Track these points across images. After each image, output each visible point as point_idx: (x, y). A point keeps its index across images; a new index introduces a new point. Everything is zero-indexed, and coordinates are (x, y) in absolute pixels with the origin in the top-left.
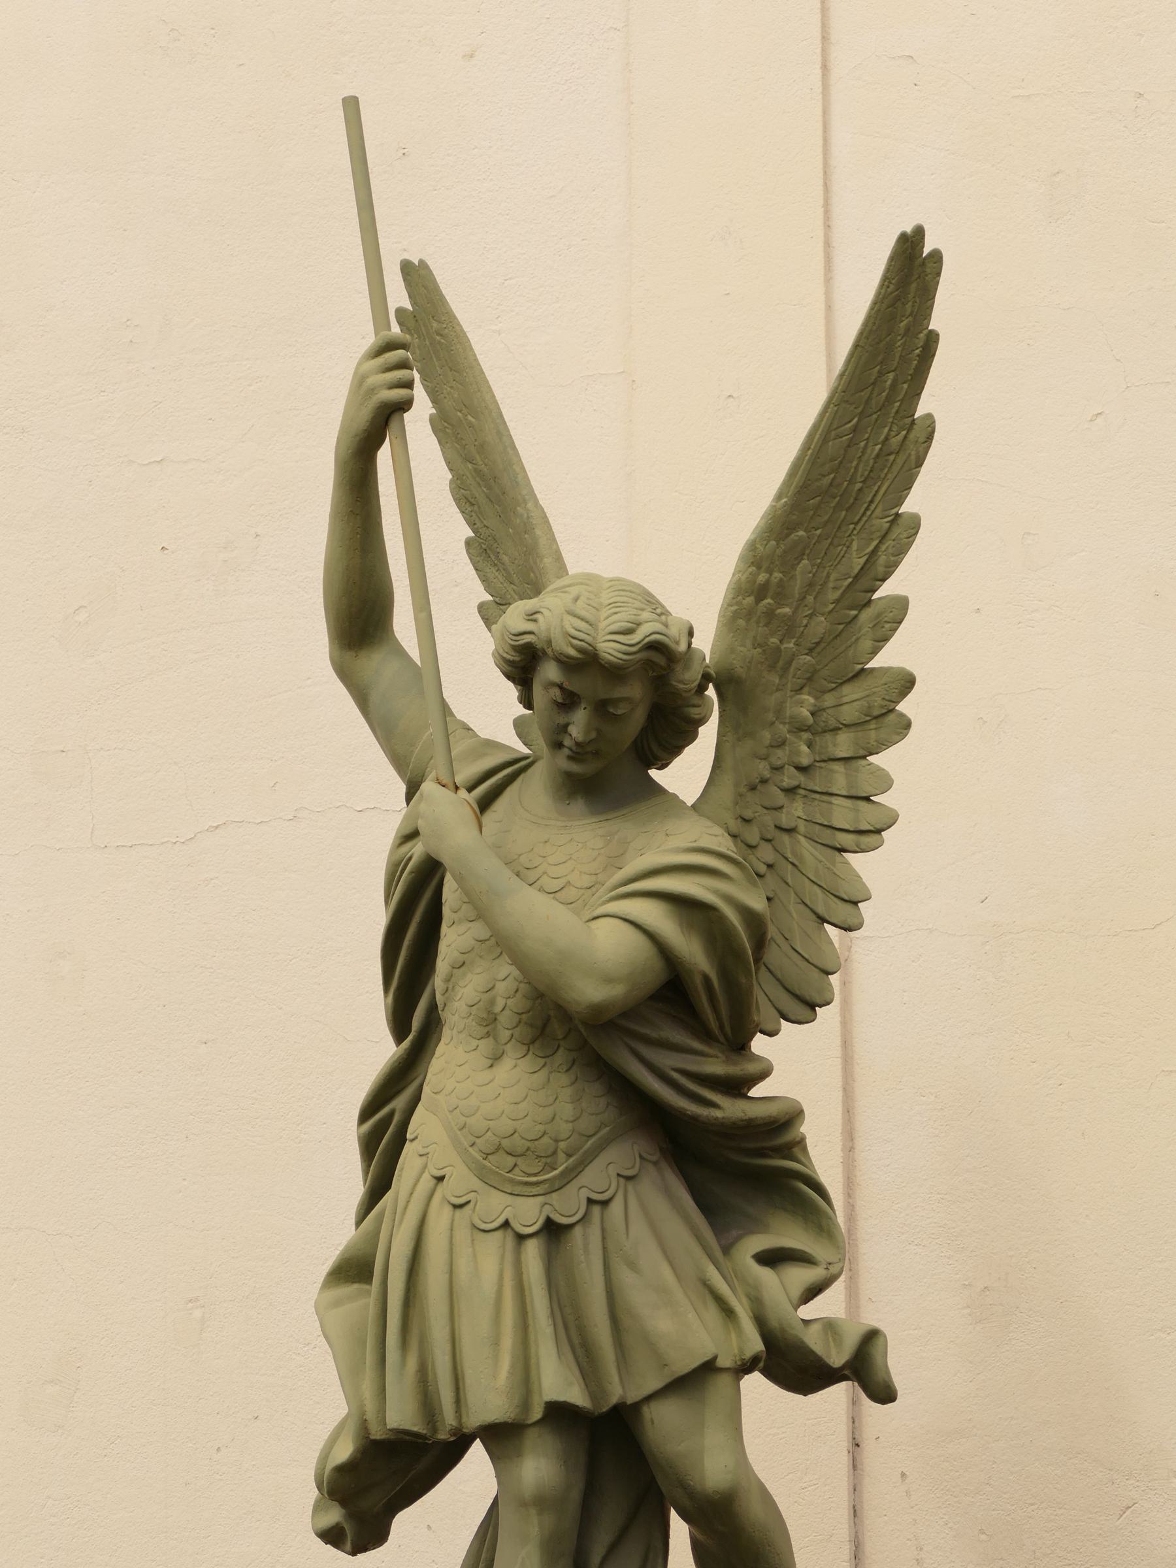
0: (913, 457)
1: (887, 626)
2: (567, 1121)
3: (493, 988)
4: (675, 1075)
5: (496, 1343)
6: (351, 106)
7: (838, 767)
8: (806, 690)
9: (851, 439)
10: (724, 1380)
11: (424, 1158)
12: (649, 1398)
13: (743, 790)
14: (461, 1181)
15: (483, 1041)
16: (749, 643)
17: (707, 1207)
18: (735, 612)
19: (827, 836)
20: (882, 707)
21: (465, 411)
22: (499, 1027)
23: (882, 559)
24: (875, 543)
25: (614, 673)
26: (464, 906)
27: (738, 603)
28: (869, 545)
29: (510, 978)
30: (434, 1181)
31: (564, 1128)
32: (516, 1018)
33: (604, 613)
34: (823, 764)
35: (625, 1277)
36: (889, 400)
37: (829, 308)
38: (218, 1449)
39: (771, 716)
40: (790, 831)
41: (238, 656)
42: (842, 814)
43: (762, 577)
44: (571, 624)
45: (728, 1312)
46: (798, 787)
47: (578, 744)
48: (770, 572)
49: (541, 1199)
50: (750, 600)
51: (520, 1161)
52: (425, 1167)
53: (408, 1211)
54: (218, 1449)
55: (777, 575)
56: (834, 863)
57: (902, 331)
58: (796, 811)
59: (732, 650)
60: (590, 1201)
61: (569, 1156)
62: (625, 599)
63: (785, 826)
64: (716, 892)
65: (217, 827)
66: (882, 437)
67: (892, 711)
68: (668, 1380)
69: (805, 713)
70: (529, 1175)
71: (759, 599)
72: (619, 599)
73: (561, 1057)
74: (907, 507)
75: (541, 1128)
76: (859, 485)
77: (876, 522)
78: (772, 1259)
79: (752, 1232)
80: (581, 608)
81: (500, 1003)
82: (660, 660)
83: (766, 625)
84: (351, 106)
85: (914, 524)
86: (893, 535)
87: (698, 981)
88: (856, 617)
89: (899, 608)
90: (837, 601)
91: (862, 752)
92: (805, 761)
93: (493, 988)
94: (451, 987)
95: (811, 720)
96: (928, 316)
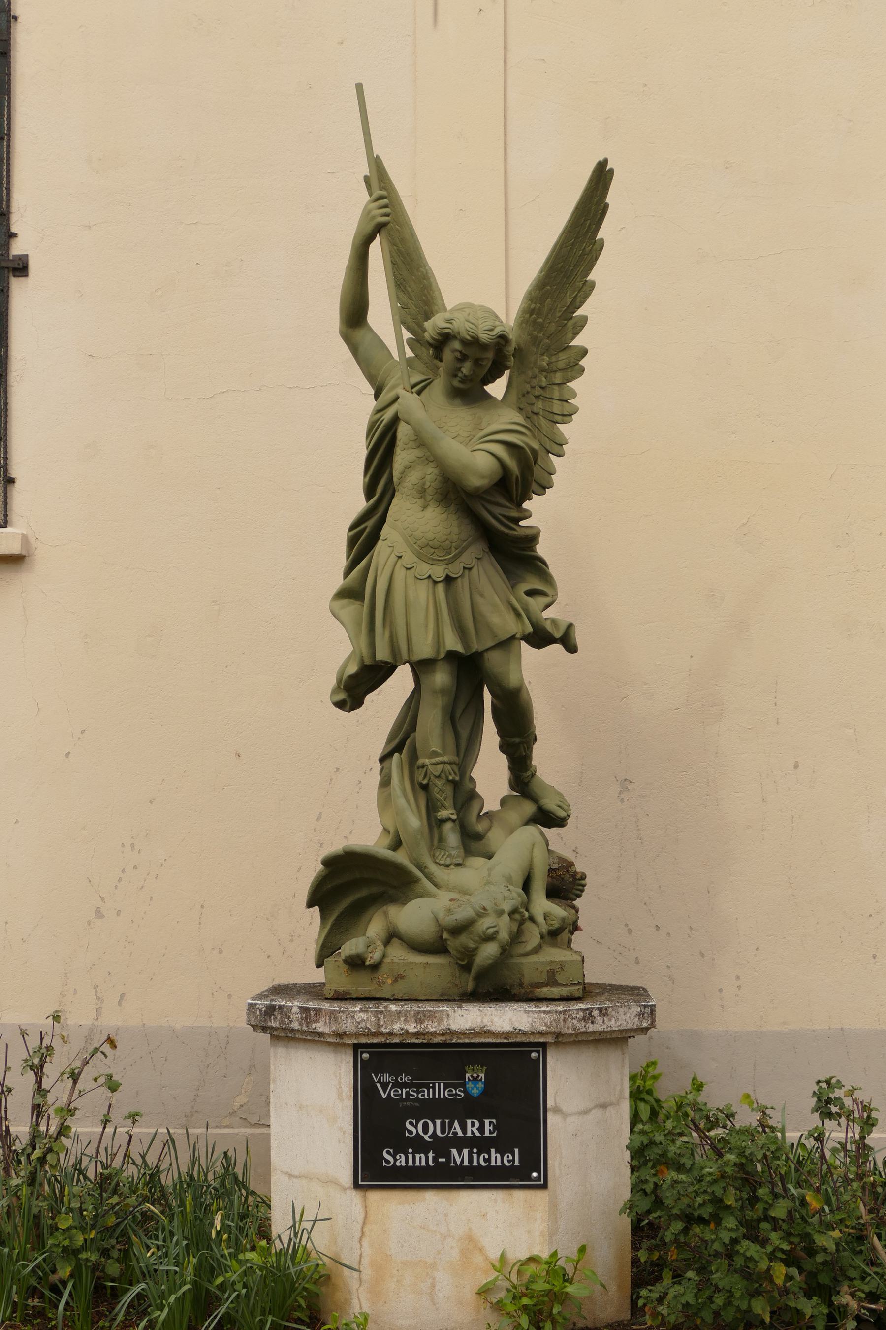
0: (594, 256)
1: (579, 328)
2: (456, 535)
3: (424, 478)
4: (500, 517)
5: (427, 626)
6: (359, 87)
7: (556, 387)
8: (546, 354)
9: (571, 248)
10: (516, 642)
11: (392, 548)
12: (487, 650)
13: (520, 396)
14: (409, 558)
15: (420, 500)
16: (526, 334)
17: (506, 572)
18: (522, 321)
19: (550, 416)
20: (574, 362)
21: (395, 223)
22: (426, 494)
23: (579, 299)
24: (576, 292)
25: (484, 347)
26: (411, 443)
27: (524, 317)
28: (573, 293)
29: (433, 474)
30: (397, 558)
31: (455, 538)
32: (435, 491)
33: (480, 322)
34: (550, 386)
35: (479, 599)
36: (587, 232)
37: (505, 172)
38: (226, 667)
39: (532, 365)
40: (537, 414)
41: (233, 315)
42: (557, 407)
43: (533, 306)
44: (468, 326)
45: (518, 615)
46: (541, 395)
47: (465, 376)
48: (535, 303)
49: (444, 567)
50: (528, 315)
51: (436, 550)
52: (393, 551)
53: (385, 571)
54: (226, 667)
55: (538, 305)
56: (553, 428)
57: (595, 203)
58: (539, 405)
59: (520, 337)
60: (464, 568)
61: (456, 549)
62: (488, 315)
63: (535, 412)
64: (522, 441)
65: (224, 392)
66: (583, 248)
67: (577, 364)
68: (497, 642)
69: (545, 364)
70: (440, 557)
71: (531, 315)
72: (486, 315)
73: (452, 508)
74: (591, 277)
75: (446, 537)
76: (572, 268)
77: (577, 284)
78: (531, 593)
79: (519, 582)
80: (471, 318)
81: (428, 484)
82: (503, 342)
83: (533, 327)
84: (359, 87)
85: (593, 285)
86: (584, 289)
87: (514, 478)
88: (566, 324)
89: (584, 320)
90: (560, 317)
91: (565, 381)
92: (544, 384)
93: (424, 478)
94: (403, 476)
95: (547, 367)
96: (605, 197)
